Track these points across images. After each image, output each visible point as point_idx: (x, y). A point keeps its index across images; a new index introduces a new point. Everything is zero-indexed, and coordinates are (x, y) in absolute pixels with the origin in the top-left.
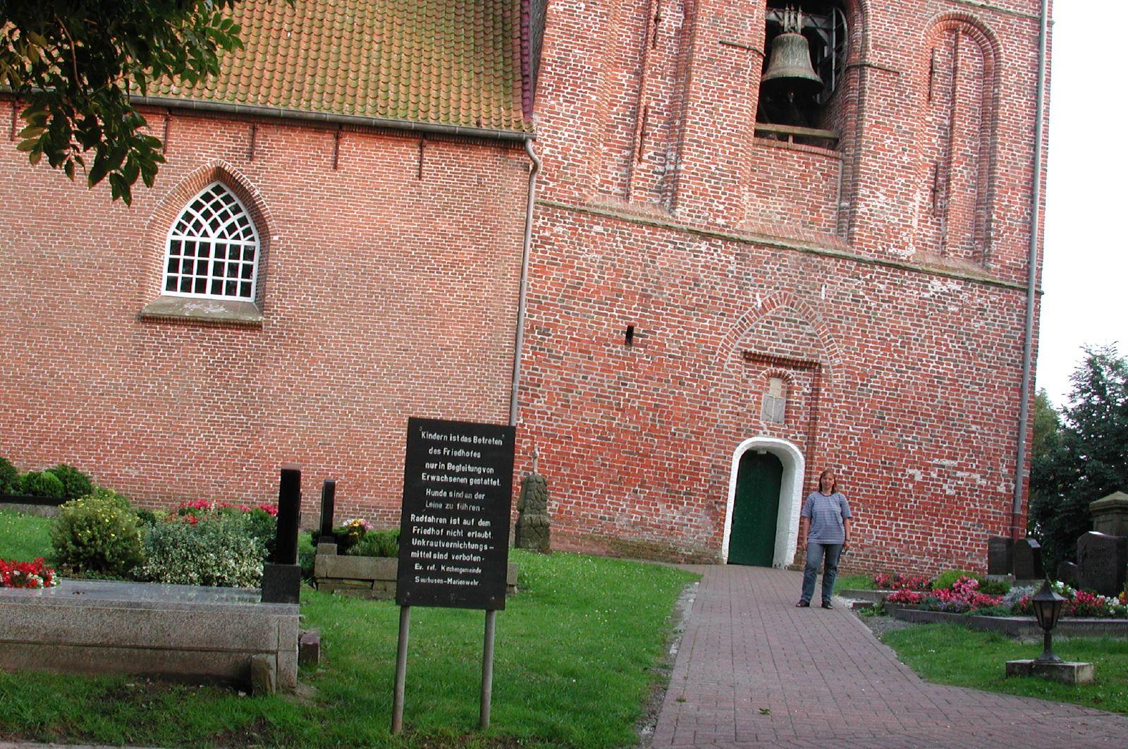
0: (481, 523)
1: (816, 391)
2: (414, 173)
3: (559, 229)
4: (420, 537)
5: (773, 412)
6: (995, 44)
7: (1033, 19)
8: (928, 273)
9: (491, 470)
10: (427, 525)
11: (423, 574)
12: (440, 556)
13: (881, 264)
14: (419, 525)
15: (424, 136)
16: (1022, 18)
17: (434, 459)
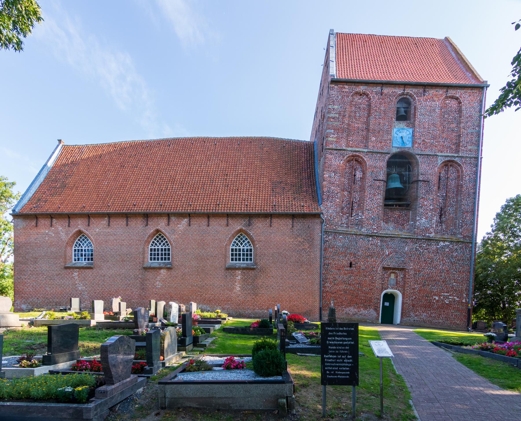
0: (349, 357)
1: (405, 276)
2: (291, 226)
3: (330, 238)
4: (328, 362)
5: (392, 283)
6: (461, 168)
7: (475, 158)
8: (439, 240)
9: (351, 339)
10: (330, 358)
11: (330, 374)
12: (335, 368)
13: (424, 239)
14: (327, 358)
15: (293, 216)
16: (471, 158)
17: (331, 336)
